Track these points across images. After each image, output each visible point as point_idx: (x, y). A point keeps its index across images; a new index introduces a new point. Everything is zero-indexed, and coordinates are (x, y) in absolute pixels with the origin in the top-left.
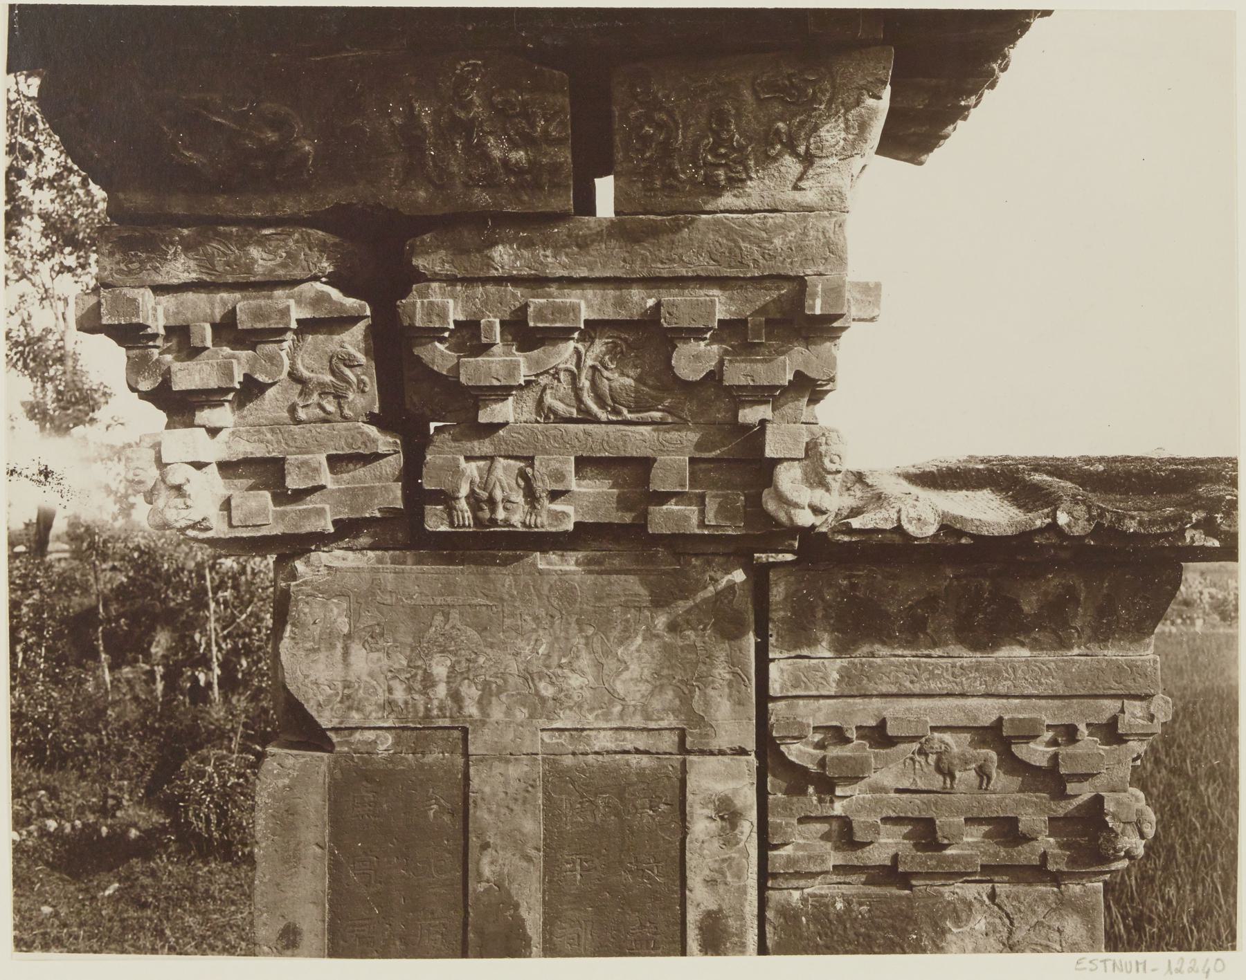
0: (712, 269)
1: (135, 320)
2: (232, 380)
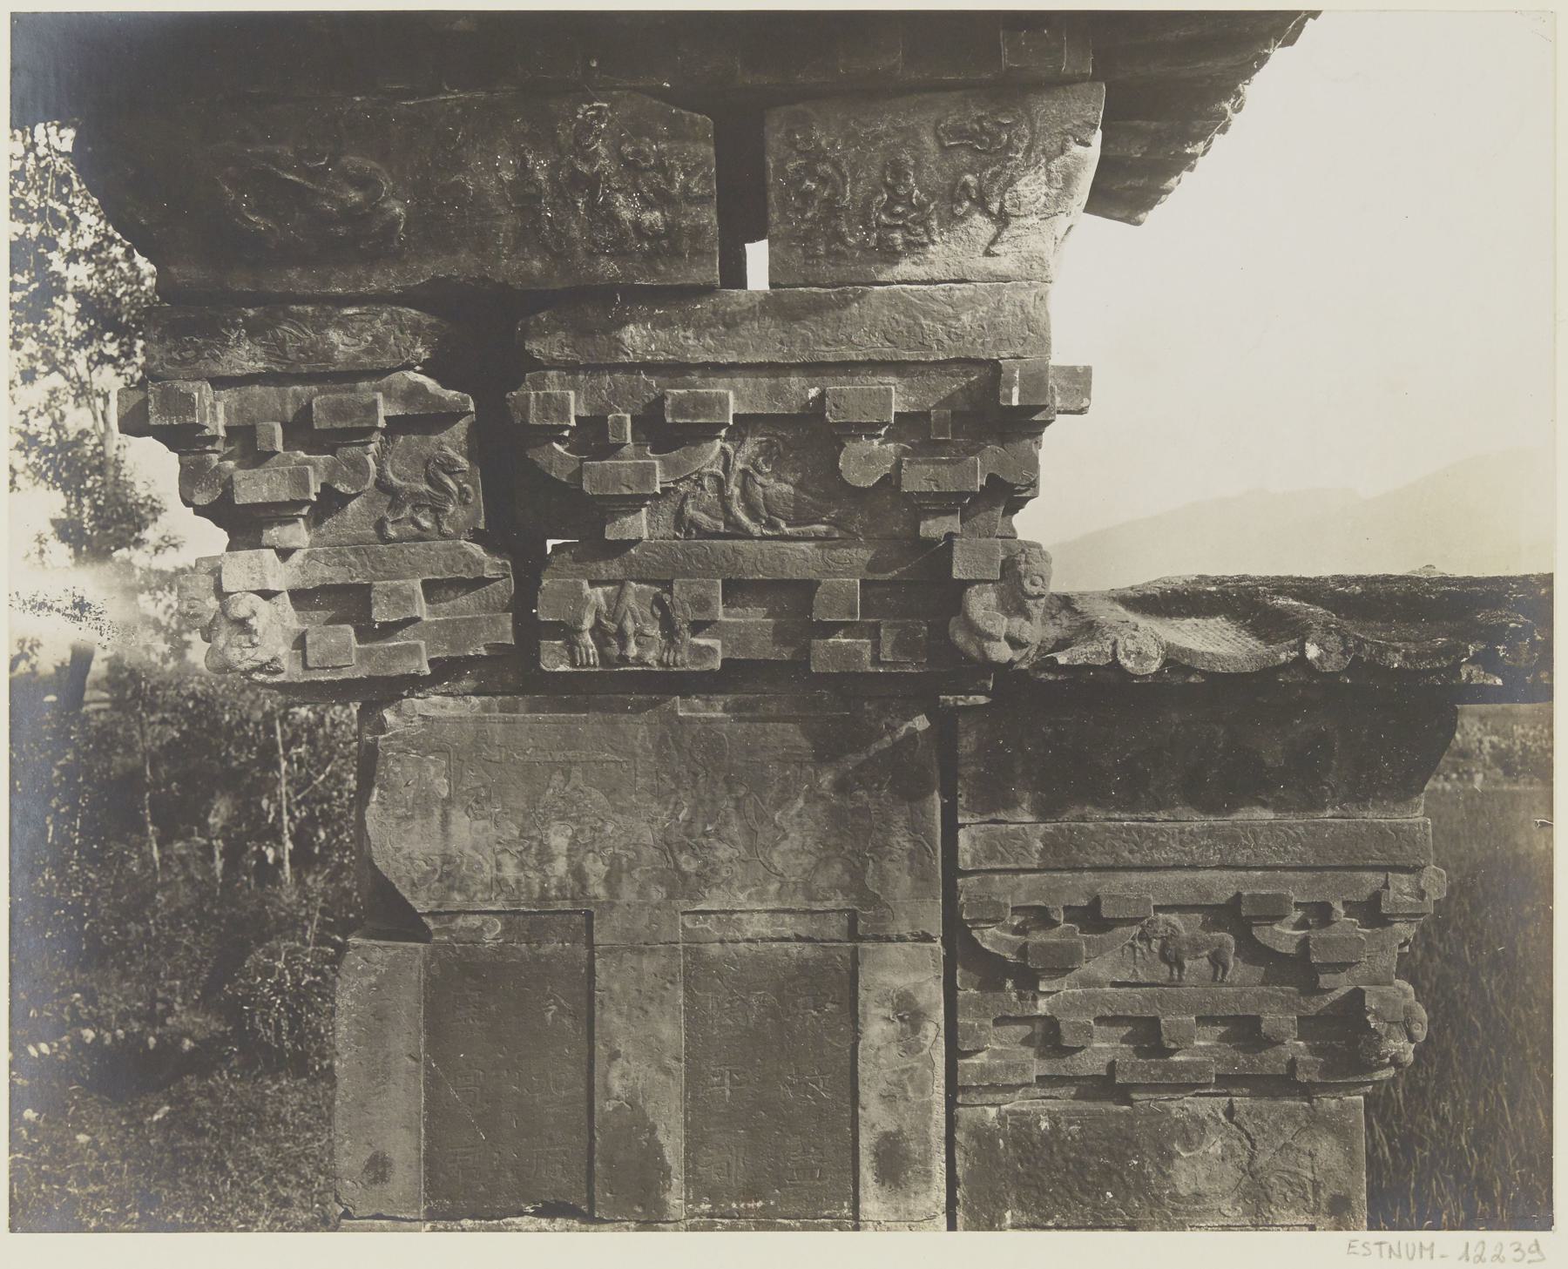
0: (888, 352)
2: (307, 490)
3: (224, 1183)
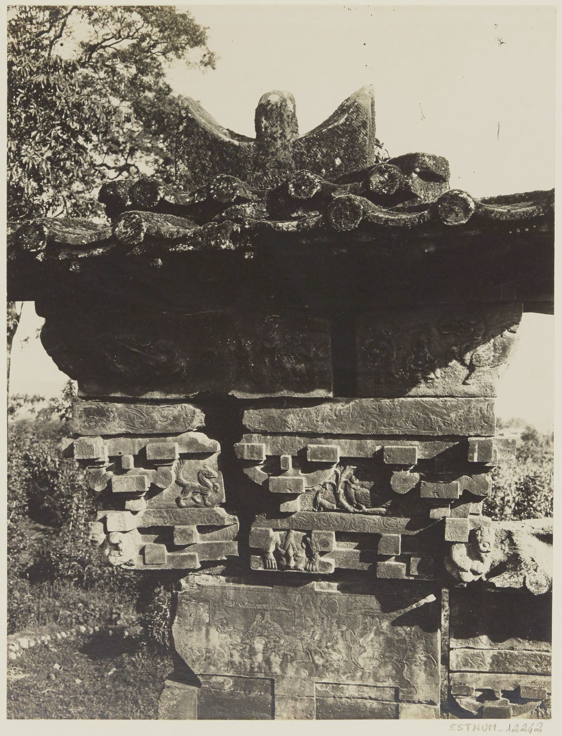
0: (413, 430)
1: (92, 457)
2: (144, 487)
3: (137, 711)
